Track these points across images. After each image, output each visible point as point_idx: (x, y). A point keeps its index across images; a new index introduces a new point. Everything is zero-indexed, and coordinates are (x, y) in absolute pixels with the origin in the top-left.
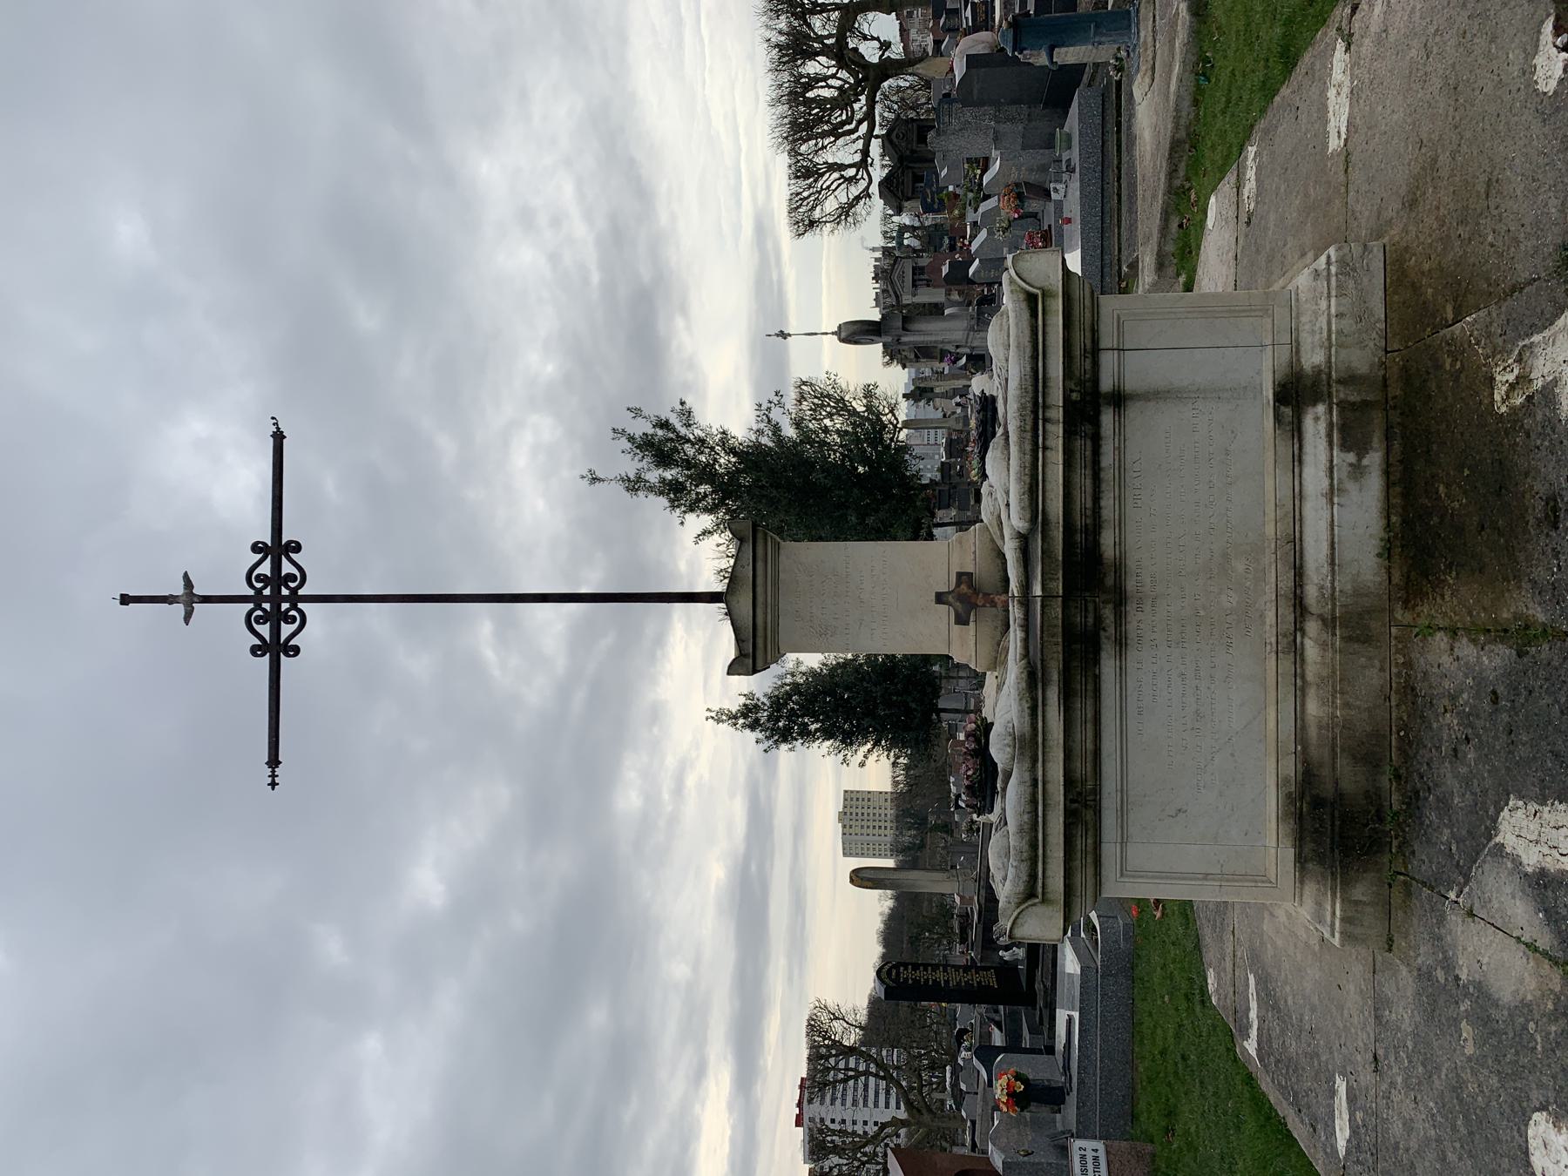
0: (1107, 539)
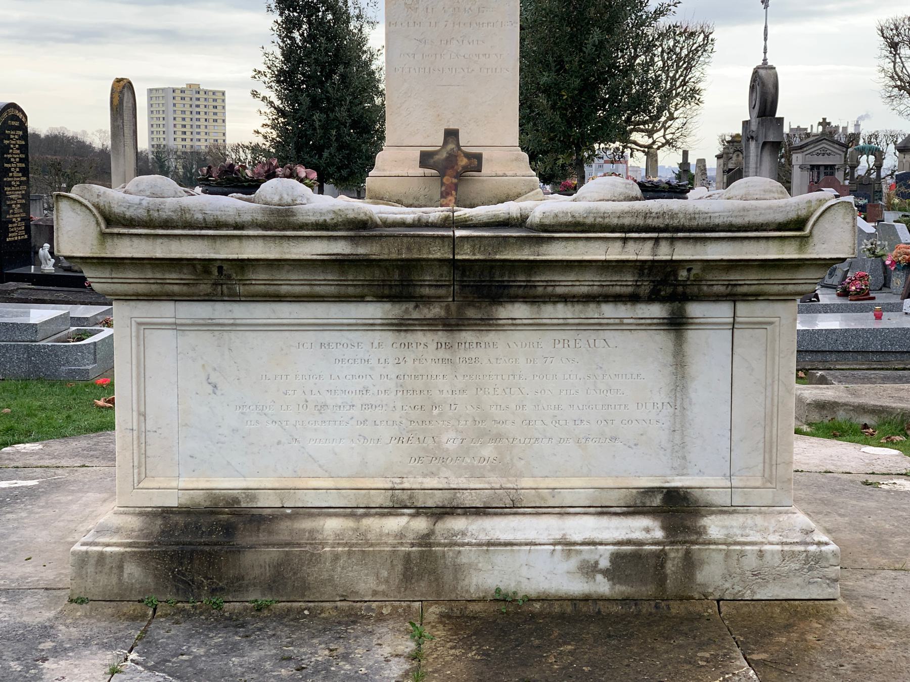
0: (519, 311)
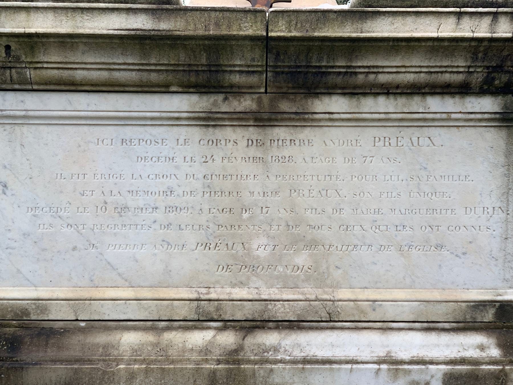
0: (337, 104)
